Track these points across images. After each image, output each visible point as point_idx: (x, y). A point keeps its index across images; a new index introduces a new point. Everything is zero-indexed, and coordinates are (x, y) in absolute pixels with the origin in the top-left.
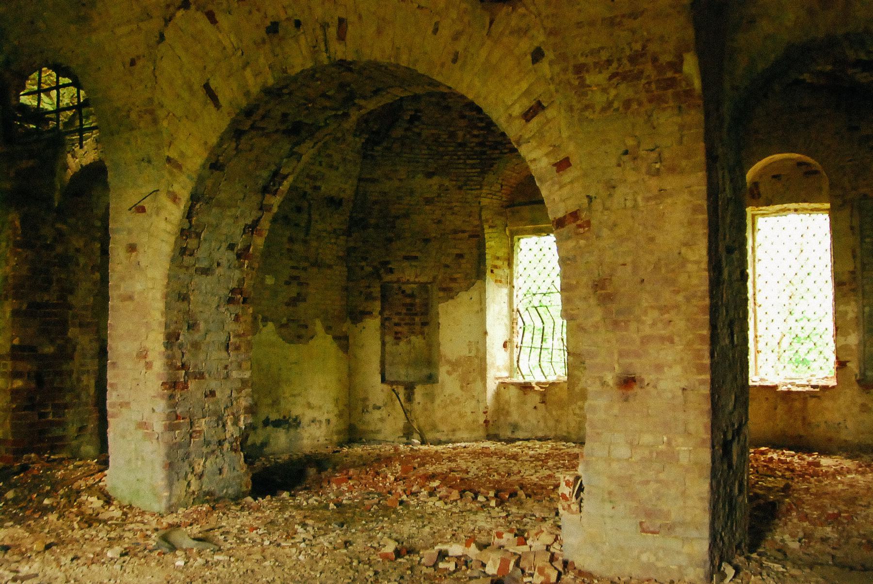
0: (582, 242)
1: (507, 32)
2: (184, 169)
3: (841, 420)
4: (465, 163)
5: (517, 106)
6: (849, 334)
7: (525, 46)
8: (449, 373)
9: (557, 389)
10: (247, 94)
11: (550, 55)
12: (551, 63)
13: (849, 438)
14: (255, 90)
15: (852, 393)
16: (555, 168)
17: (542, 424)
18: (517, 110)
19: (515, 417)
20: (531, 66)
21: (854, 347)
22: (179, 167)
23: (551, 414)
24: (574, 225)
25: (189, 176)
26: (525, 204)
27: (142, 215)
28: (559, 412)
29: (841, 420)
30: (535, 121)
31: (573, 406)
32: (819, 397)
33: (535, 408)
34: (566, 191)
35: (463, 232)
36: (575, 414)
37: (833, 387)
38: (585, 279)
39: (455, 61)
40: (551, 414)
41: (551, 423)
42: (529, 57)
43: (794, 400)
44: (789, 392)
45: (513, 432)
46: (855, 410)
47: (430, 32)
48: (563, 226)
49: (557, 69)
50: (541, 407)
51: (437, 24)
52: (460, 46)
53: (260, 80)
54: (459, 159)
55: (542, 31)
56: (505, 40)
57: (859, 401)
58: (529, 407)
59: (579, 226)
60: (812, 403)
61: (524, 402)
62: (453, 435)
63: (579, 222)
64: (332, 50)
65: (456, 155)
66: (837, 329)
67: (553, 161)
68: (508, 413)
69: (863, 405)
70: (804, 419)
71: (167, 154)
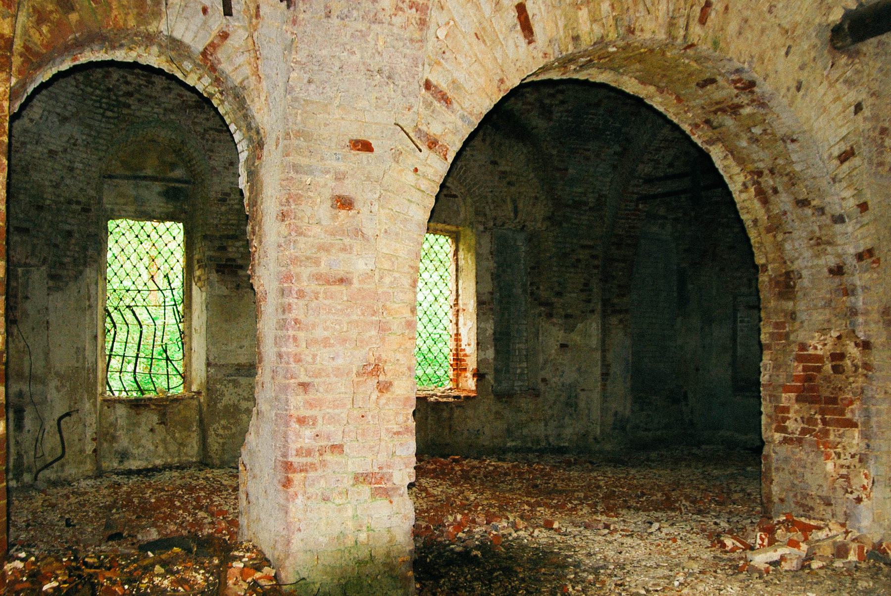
0: (875, 275)
1: (841, 80)
2: (455, 105)
3: (480, 427)
4: (103, 115)
5: (837, 147)
6: (488, 349)
7: (852, 96)
8: (58, 389)
9: (181, 407)
10: (576, 39)
11: (867, 112)
12: (865, 119)
13: (486, 443)
14: (586, 42)
15: (489, 401)
16: (859, 209)
17: (161, 450)
18: (836, 152)
19: (124, 442)
20: (852, 116)
21: (491, 361)
22: (446, 100)
23: (173, 437)
24: (870, 260)
25: (463, 117)
26: (127, 178)
27: (364, 155)
28: (185, 433)
29: (480, 427)
30: (847, 164)
31: (215, 426)
32: (462, 407)
33: (152, 430)
34: (864, 230)
35: (78, 203)
36: (217, 435)
37: (474, 397)
38: (876, 307)
39: (798, 89)
40: (173, 437)
41: (173, 448)
42: (853, 108)
43: (443, 410)
44: (437, 403)
45: (121, 462)
46: (491, 417)
47: (783, 53)
48: (862, 260)
49: (869, 125)
50: (160, 429)
51: (790, 47)
52: (804, 76)
53: (598, 30)
54: (101, 107)
55: (867, 90)
56: (838, 85)
57: (494, 409)
58: (143, 430)
59: (874, 262)
60: (457, 412)
61: (138, 424)
62: (63, 471)
63: (874, 258)
64: (691, 30)
65: (99, 101)
66: (478, 344)
67: (857, 203)
68: (114, 438)
69: (497, 413)
70: (450, 427)
71: (427, 75)
